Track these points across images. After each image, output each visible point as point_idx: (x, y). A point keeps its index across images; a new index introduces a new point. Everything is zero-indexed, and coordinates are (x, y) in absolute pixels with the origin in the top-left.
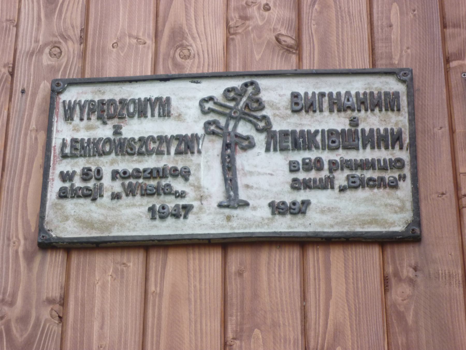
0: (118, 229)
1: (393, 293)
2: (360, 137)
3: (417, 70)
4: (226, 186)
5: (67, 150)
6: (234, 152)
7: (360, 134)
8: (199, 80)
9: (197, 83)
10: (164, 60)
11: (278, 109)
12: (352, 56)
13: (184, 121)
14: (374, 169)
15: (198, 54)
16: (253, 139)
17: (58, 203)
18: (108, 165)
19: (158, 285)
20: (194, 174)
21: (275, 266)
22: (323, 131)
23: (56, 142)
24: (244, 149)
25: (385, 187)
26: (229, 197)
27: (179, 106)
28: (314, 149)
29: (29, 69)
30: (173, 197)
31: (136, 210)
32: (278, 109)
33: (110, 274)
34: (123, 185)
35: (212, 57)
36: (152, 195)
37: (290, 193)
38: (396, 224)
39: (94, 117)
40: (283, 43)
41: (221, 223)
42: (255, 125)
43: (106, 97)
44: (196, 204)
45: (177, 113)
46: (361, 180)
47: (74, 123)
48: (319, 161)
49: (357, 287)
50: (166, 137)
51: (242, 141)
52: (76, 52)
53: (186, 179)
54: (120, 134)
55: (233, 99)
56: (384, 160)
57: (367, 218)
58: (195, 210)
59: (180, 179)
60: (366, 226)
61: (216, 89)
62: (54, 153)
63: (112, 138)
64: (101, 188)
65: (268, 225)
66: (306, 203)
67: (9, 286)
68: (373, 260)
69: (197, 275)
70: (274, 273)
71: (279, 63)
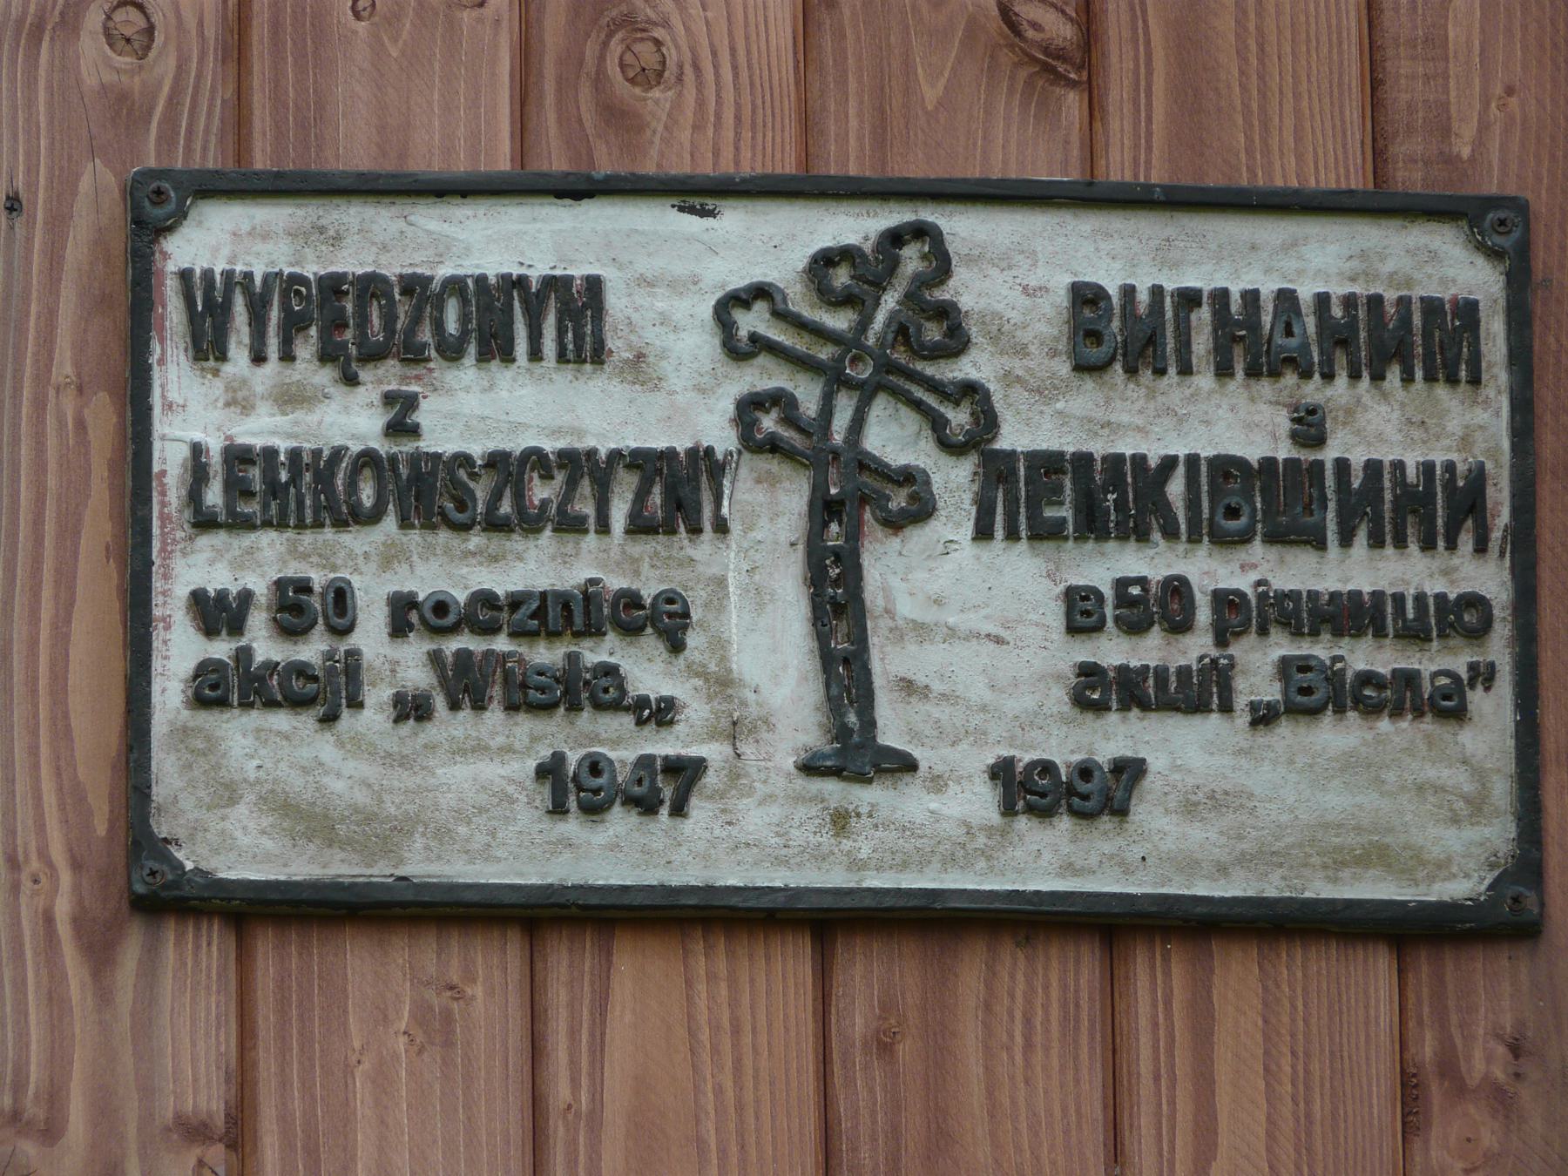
0: (427, 848)
1: (1433, 1142)
2: (1330, 494)
3: (1544, 192)
4: (827, 686)
5: (214, 496)
6: (854, 535)
7: (1330, 481)
8: (710, 203)
9: (704, 213)
10: (560, 81)
11: (1022, 351)
12: (1297, 111)
13: (654, 383)
14: (1380, 633)
15: (697, 68)
16: (927, 482)
17: (191, 724)
18: (373, 566)
19: (584, 1081)
20: (701, 624)
21: (1012, 1018)
22: (1193, 461)
23: (169, 458)
24: (896, 524)
25: (1419, 713)
26: (841, 733)
27: (635, 317)
28: (1156, 536)
29: (30, 103)
30: (628, 720)
31: (492, 771)
32: (1022, 351)
33: (403, 1028)
34: (435, 658)
35: (752, 85)
36: (547, 708)
37: (1064, 720)
38: (1455, 869)
39: (305, 349)
40: (1030, 34)
41: (813, 840)
42: (937, 424)
43: (352, 262)
44: (713, 752)
45: (630, 347)
46: (1334, 677)
47: (228, 369)
48: (1177, 588)
49: (1308, 1116)
50: (591, 453)
51: (888, 489)
52: (211, 32)
53: (676, 646)
54: (414, 431)
55: (846, 300)
56: (1420, 598)
57: (1351, 840)
58: (711, 779)
59: (650, 642)
60: (1346, 874)
61: (772, 244)
62: (163, 504)
63: (383, 447)
64: (352, 667)
65: (989, 858)
66: (1130, 771)
67: (33, 1059)
68: (1366, 1007)
69: (727, 1046)
70: (1009, 1049)
71: (1014, 129)
